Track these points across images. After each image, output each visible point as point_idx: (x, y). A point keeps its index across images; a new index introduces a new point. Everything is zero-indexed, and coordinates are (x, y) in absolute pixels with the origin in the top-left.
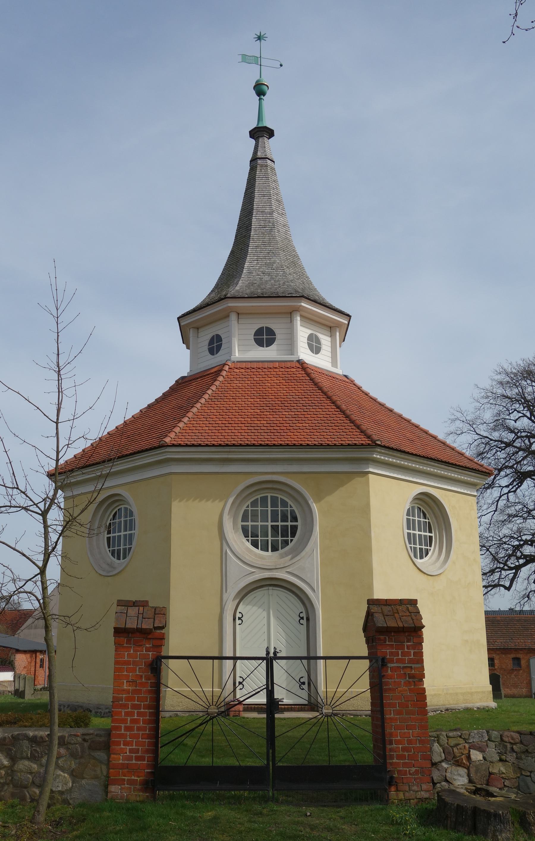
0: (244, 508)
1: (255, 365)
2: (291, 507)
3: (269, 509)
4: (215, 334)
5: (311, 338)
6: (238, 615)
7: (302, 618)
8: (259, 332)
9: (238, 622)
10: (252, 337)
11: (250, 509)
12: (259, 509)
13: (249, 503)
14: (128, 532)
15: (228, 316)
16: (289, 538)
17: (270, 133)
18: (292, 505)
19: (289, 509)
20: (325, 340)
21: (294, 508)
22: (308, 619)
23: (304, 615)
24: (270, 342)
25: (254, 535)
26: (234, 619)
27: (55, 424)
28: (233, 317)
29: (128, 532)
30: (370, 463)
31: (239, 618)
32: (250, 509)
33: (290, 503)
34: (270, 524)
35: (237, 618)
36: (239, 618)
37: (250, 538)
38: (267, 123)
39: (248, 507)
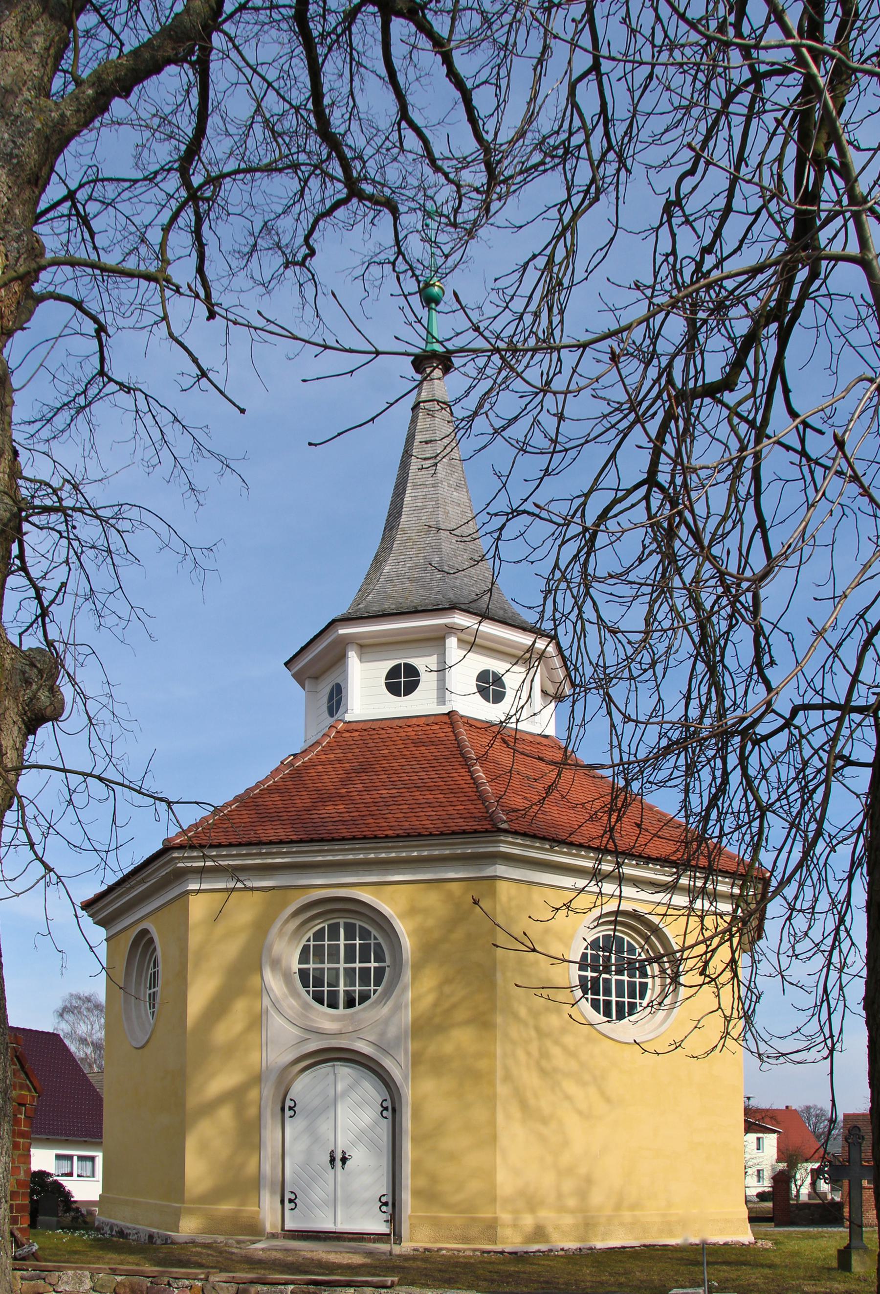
0: (303, 942)
1: (414, 721)
2: (375, 938)
3: (342, 942)
4: (334, 683)
5: (483, 676)
6: (288, 1103)
7: (386, 1109)
8: (394, 673)
9: (288, 1113)
10: (383, 681)
11: (372, 988)
12: (326, 943)
13: (310, 934)
14: (152, 990)
15: (342, 658)
16: (312, 943)
18: (378, 936)
19: (372, 942)
20: (424, 663)
21: (381, 940)
22: (394, 1110)
23: (388, 1104)
24: (411, 687)
25: (318, 982)
26: (283, 1109)
27: (858, 270)
28: (353, 657)
29: (152, 990)
30: (499, 861)
31: (290, 1108)
32: (312, 943)
33: (374, 932)
34: (342, 965)
35: (287, 1108)
36: (290, 1108)
37: (311, 989)
39: (309, 940)
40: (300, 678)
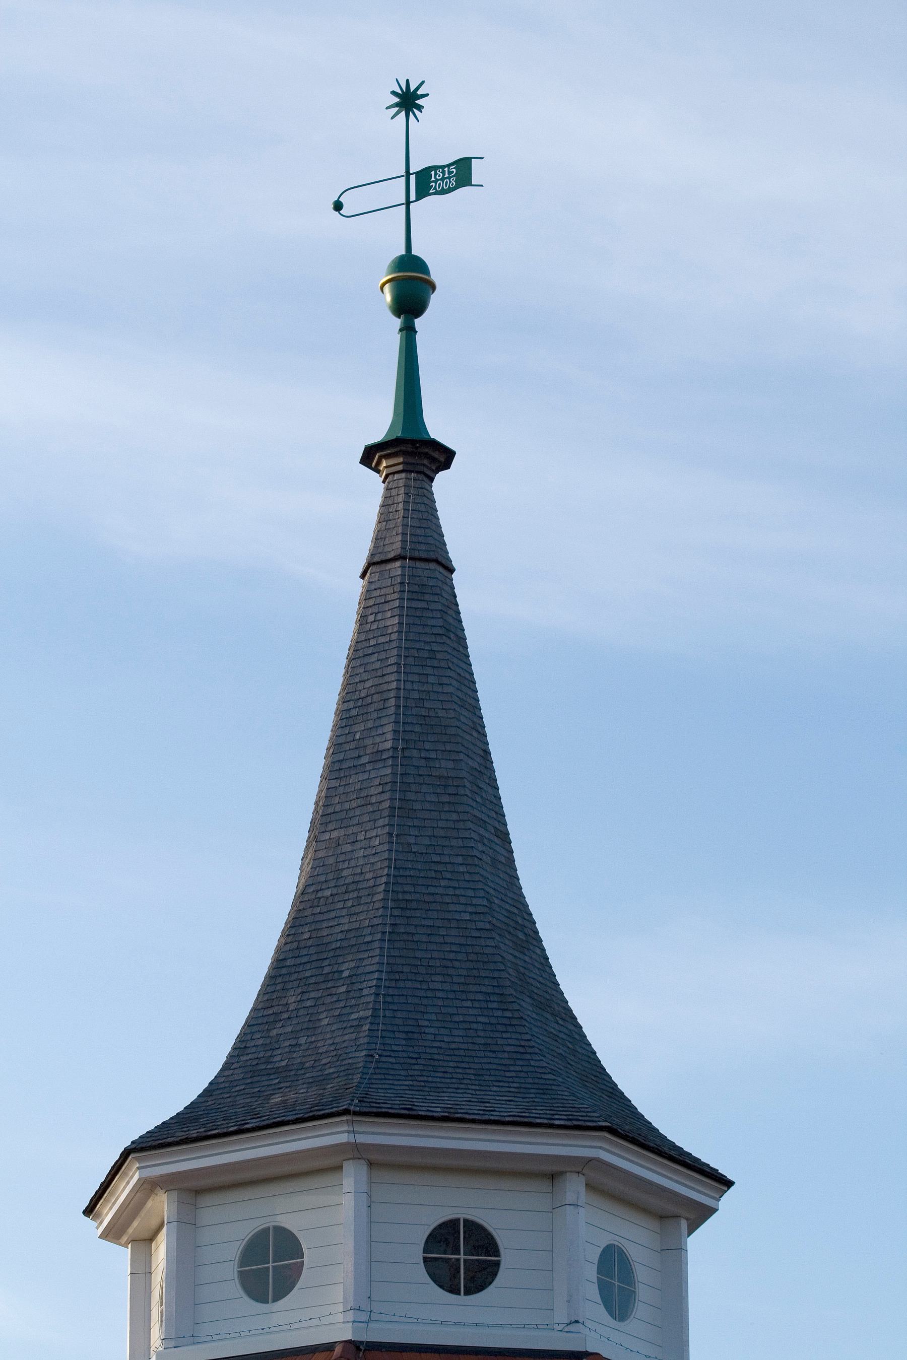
8: (444, 1236)
10: (418, 1254)
17: (443, 457)
38: (437, 426)
40: (113, 1233)
